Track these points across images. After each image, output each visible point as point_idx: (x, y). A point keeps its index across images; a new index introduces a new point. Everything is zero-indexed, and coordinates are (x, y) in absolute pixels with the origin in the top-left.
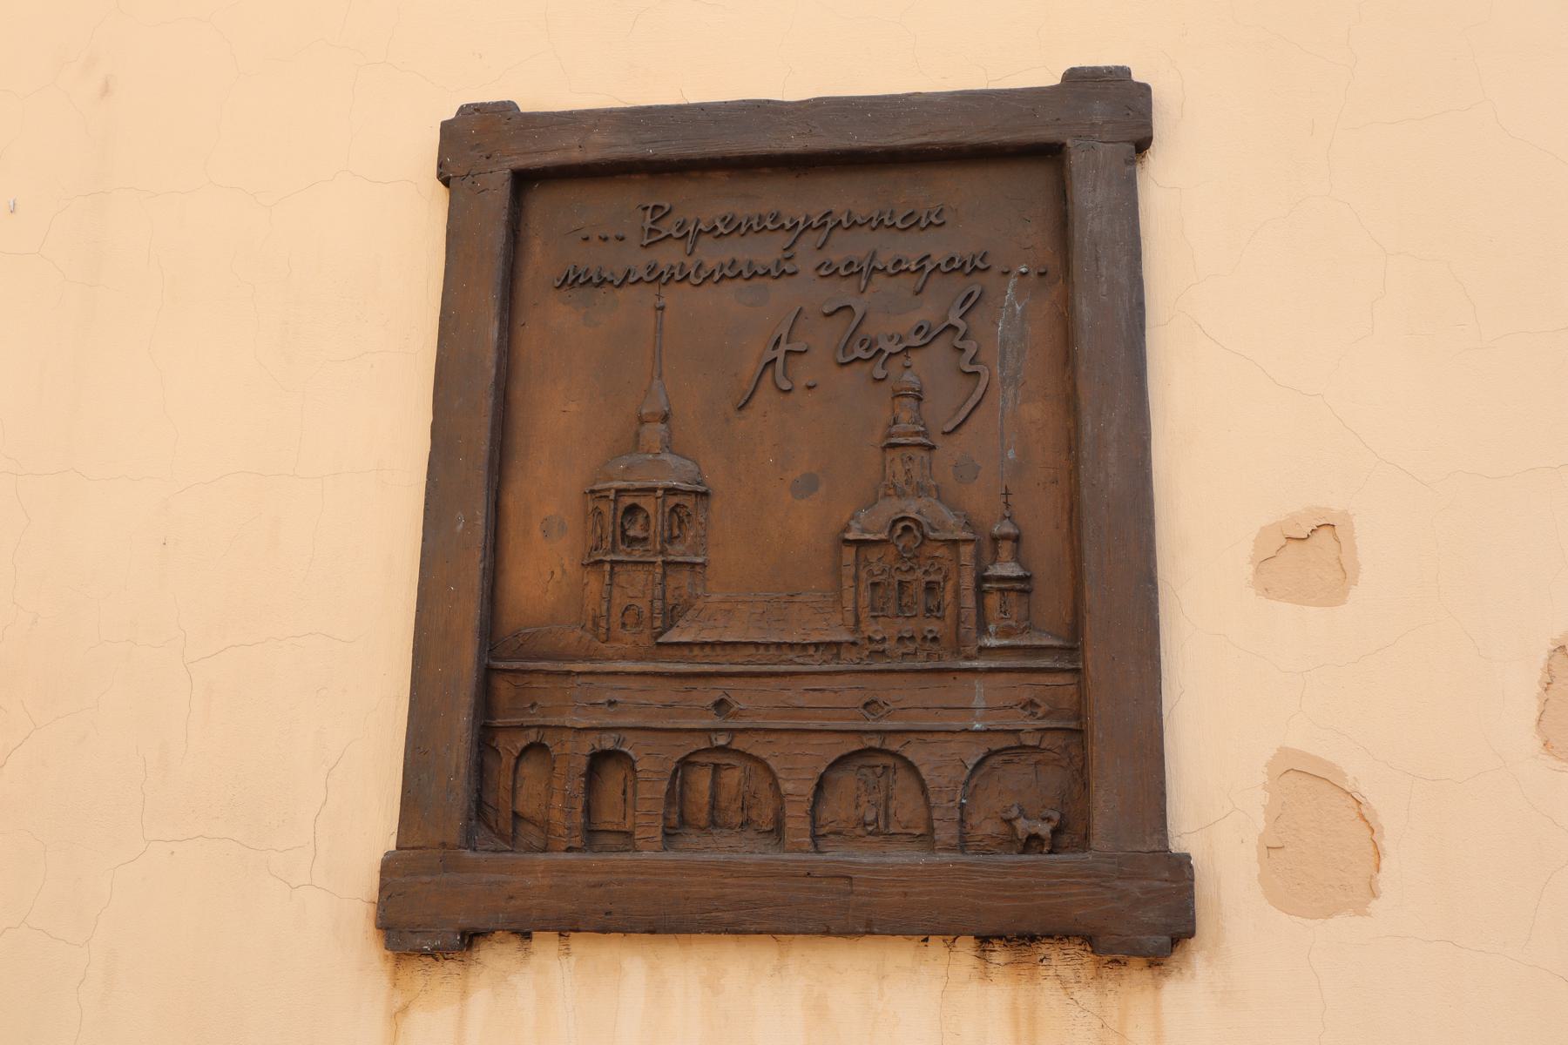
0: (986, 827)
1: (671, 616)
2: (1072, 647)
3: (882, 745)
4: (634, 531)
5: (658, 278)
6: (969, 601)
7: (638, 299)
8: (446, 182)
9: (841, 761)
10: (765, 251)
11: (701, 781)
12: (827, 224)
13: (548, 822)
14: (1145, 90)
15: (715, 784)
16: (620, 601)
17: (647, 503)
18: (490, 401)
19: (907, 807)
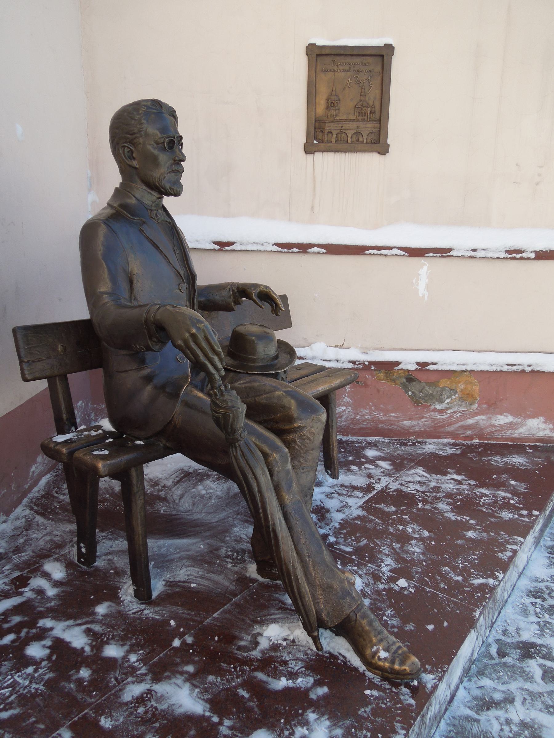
0: (369, 141)
1: (336, 116)
2: (380, 121)
3: (321, 461)
4: (332, 105)
5: (334, 71)
6: (369, 115)
7: (331, 73)
8: (307, 55)
9: (354, 133)
10: (347, 67)
11: (340, 135)
12: (355, 64)
13: (483, 674)
14: (394, 47)
15: (341, 135)
16: (330, 114)
17: (333, 102)
18: (460, 674)
19: (361, 139)
